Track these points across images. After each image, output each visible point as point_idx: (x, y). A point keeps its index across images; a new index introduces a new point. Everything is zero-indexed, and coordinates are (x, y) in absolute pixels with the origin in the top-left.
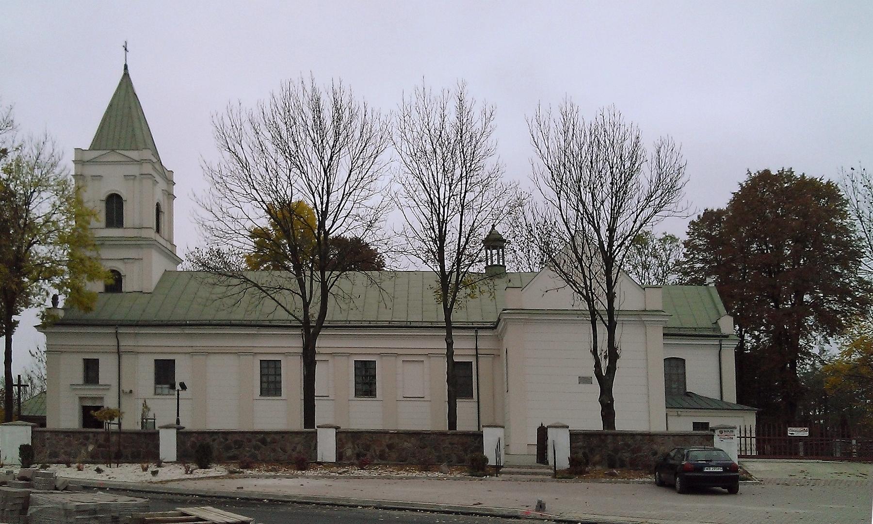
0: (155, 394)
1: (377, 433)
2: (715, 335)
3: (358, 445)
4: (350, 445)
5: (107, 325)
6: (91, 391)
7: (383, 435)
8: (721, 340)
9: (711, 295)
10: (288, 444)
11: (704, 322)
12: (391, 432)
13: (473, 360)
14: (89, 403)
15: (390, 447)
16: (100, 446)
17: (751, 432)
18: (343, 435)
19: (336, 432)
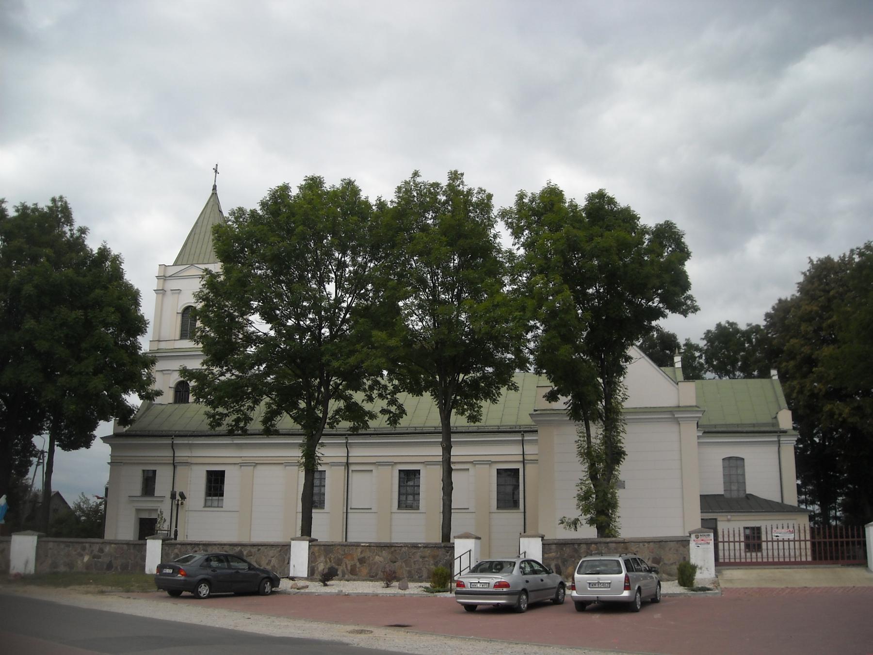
0: (205, 506)
1: (349, 546)
2: (774, 431)
3: (330, 559)
4: (322, 559)
5: (153, 436)
6: (147, 504)
7: (354, 547)
8: (780, 436)
9: (774, 388)
10: (263, 557)
11: (764, 418)
12: (362, 544)
13: (519, 466)
14: (145, 516)
15: (362, 561)
16: (94, 557)
17: (729, 536)
18: (316, 549)
19: (309, 545)
